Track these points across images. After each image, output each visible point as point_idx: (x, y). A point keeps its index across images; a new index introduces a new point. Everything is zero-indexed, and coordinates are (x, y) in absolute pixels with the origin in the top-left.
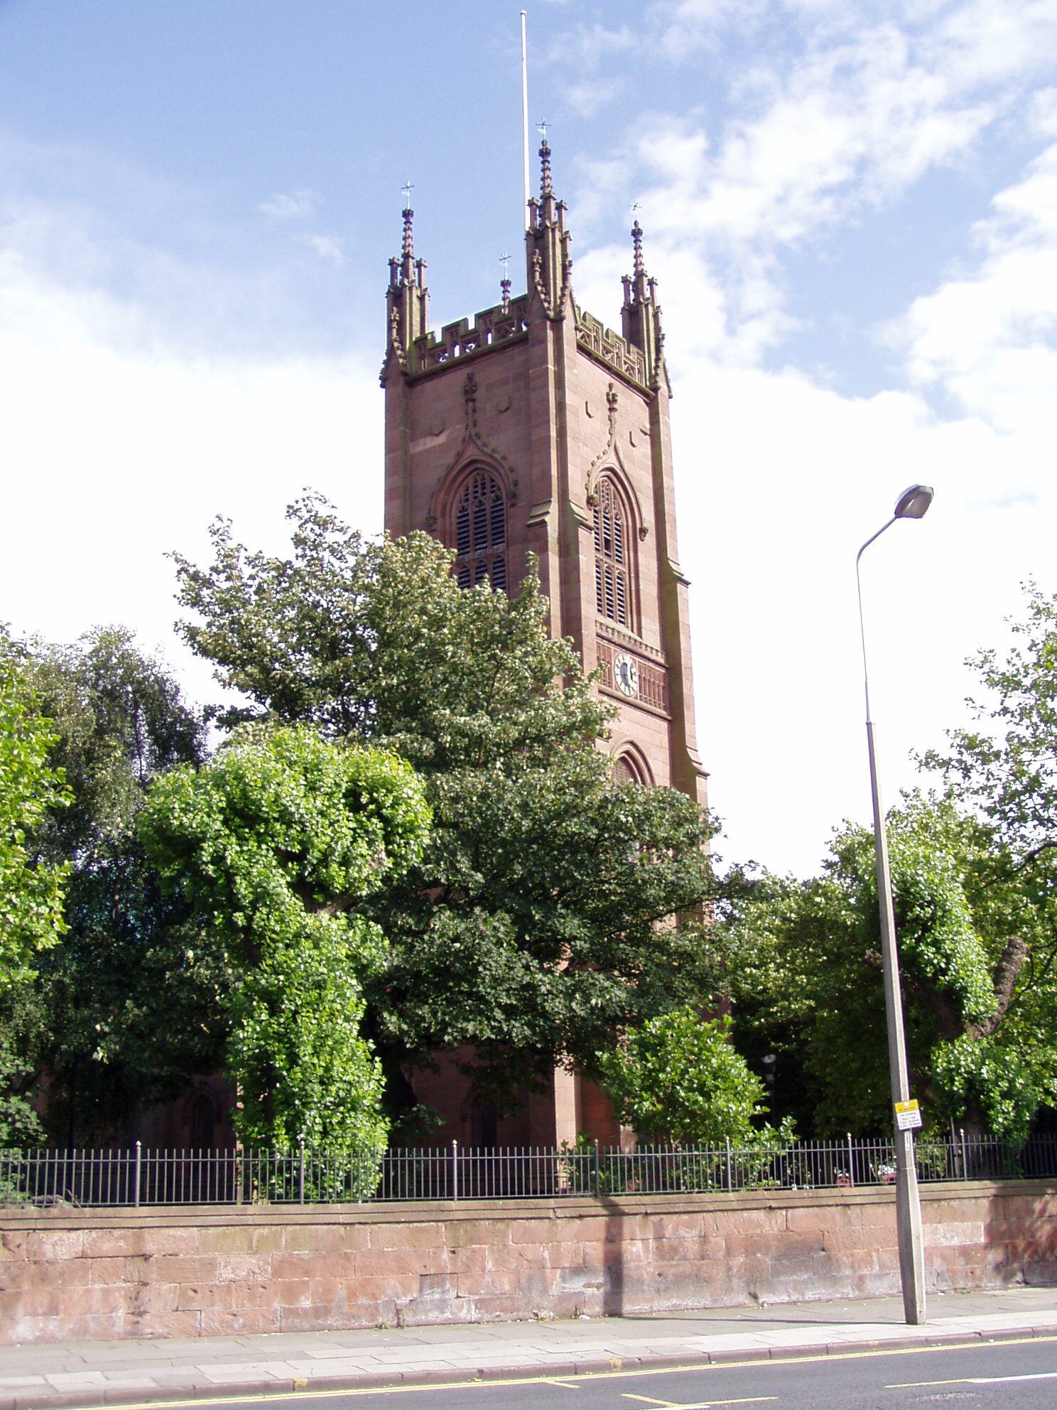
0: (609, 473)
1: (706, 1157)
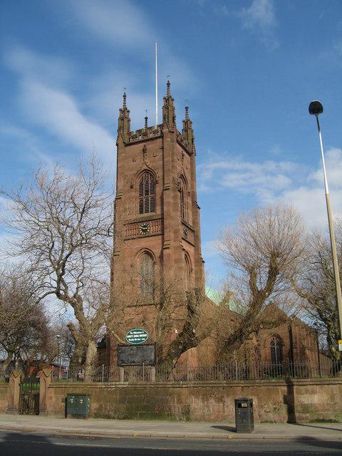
1: (188, 177)
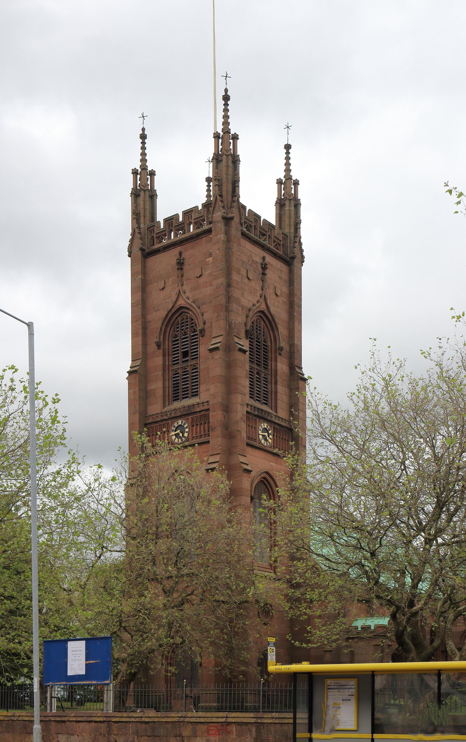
0: (261, 314)
1: (278, 310)
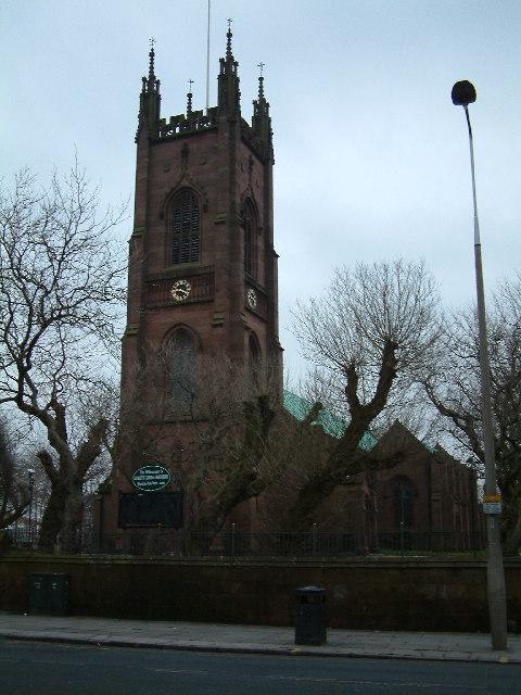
1: (259, 200)
